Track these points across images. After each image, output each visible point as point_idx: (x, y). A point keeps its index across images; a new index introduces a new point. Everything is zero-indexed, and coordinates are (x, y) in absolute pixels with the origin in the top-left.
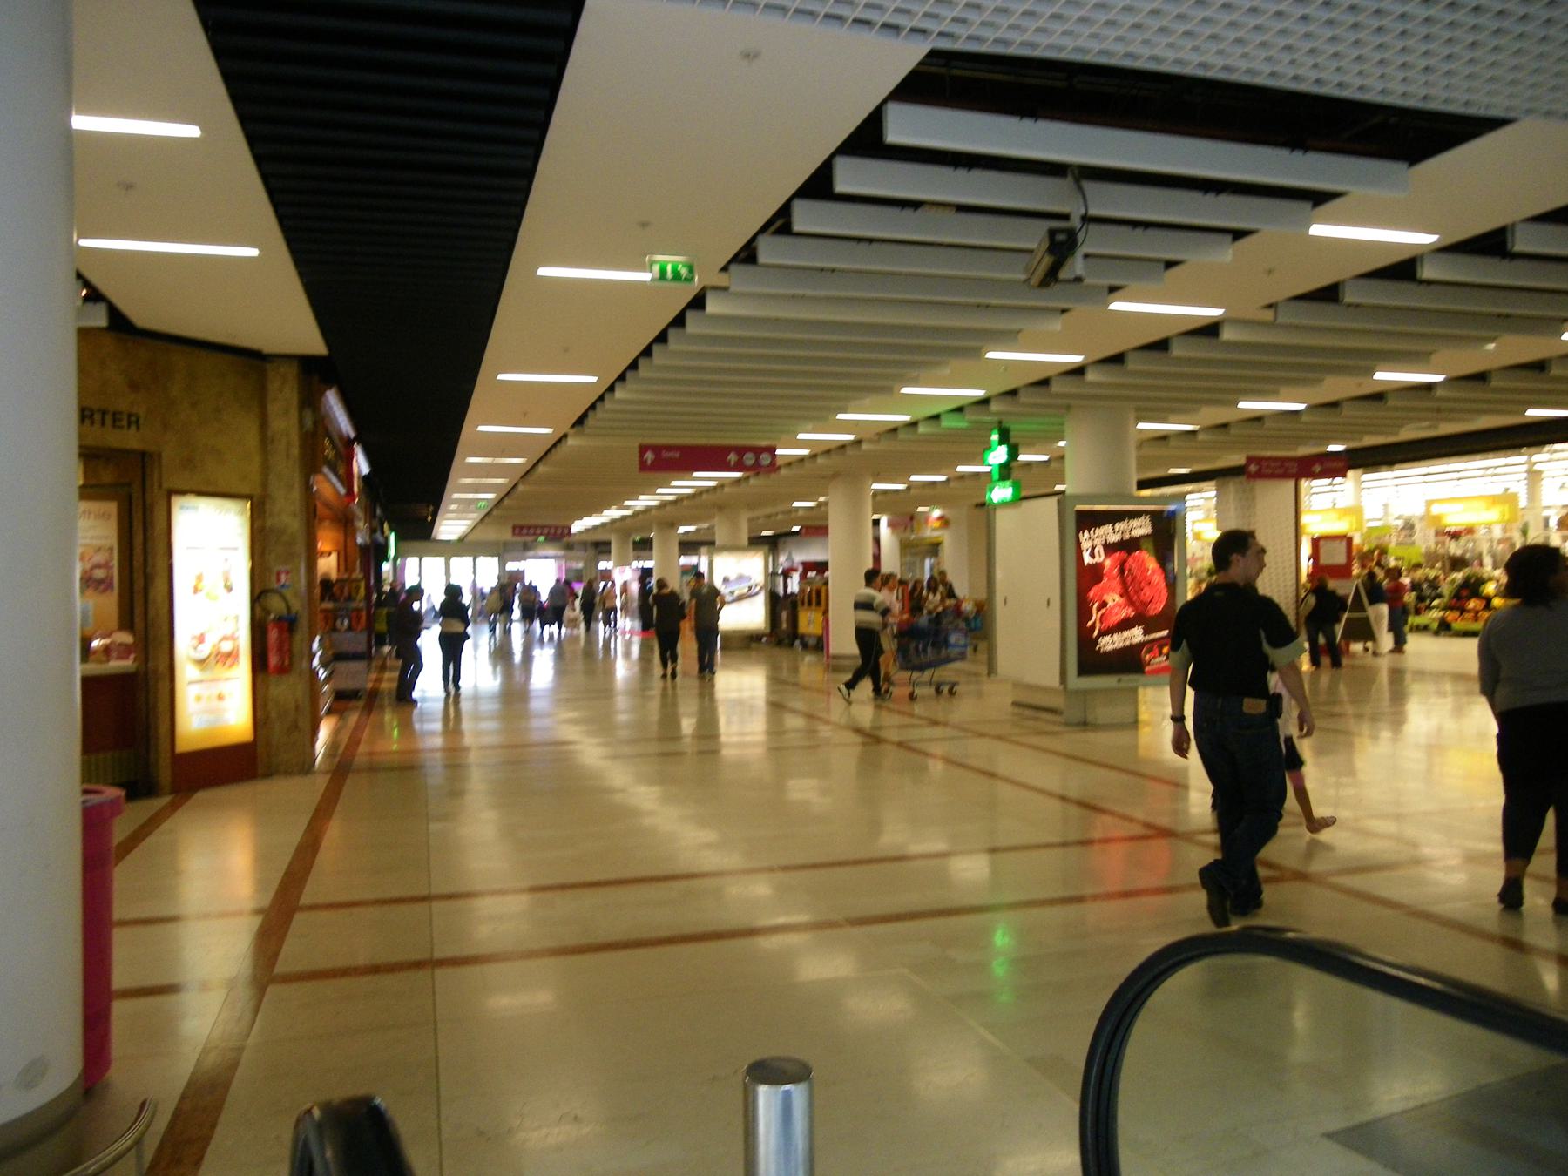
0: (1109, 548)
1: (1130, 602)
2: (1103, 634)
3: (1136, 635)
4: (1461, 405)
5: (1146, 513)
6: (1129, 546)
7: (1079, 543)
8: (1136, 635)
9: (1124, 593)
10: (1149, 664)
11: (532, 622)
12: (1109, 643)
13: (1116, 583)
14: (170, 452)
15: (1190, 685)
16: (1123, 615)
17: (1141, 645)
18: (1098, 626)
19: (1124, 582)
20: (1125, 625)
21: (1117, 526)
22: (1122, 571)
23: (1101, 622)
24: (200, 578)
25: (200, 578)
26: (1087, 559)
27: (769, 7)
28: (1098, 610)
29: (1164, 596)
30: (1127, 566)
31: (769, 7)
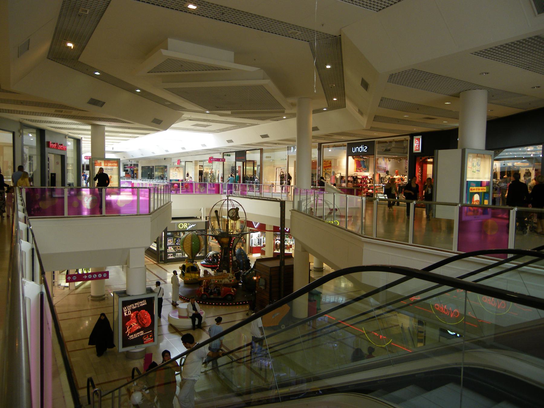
0: (133, 311)
1: (139, 324)
2: (130, 335)
3: (142, 333)
4: (522, 153)
5: (144, 299)
6: (139, 309)
7: (123, 310)
8: (142, 333)
9: (138, 322)
10: (145, 340)
11: (427, 161)
12: (132, 337)
13: (135, 320)
14: (177, 187)
15: (292, 291)
16: (137, 328)
17: (143, 335)
18: (129, 332)
19: (137, 319)
20: (138, 331)
21: (135, 304)
22: (137, 316)
23: (130, 332)
24: (532, 88)
25: (532, 88)
26: (125, 314)
27: (142, 1)
28: (129, 328)
29: (150, 321)
30: (138, 315)
31: (142, 1)
